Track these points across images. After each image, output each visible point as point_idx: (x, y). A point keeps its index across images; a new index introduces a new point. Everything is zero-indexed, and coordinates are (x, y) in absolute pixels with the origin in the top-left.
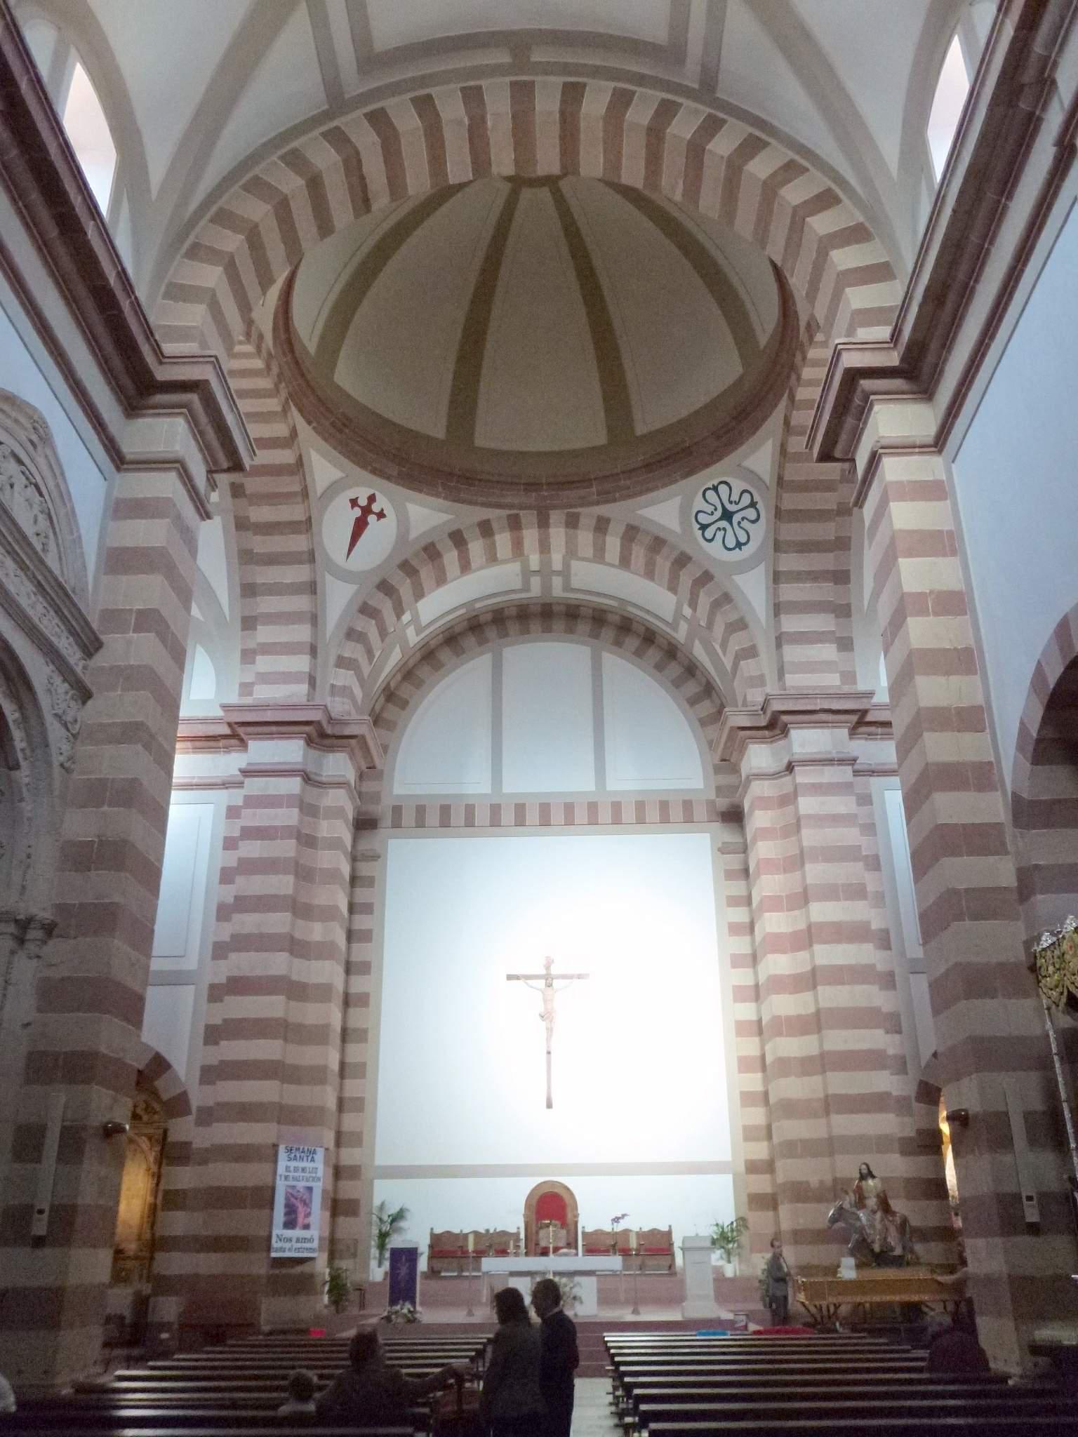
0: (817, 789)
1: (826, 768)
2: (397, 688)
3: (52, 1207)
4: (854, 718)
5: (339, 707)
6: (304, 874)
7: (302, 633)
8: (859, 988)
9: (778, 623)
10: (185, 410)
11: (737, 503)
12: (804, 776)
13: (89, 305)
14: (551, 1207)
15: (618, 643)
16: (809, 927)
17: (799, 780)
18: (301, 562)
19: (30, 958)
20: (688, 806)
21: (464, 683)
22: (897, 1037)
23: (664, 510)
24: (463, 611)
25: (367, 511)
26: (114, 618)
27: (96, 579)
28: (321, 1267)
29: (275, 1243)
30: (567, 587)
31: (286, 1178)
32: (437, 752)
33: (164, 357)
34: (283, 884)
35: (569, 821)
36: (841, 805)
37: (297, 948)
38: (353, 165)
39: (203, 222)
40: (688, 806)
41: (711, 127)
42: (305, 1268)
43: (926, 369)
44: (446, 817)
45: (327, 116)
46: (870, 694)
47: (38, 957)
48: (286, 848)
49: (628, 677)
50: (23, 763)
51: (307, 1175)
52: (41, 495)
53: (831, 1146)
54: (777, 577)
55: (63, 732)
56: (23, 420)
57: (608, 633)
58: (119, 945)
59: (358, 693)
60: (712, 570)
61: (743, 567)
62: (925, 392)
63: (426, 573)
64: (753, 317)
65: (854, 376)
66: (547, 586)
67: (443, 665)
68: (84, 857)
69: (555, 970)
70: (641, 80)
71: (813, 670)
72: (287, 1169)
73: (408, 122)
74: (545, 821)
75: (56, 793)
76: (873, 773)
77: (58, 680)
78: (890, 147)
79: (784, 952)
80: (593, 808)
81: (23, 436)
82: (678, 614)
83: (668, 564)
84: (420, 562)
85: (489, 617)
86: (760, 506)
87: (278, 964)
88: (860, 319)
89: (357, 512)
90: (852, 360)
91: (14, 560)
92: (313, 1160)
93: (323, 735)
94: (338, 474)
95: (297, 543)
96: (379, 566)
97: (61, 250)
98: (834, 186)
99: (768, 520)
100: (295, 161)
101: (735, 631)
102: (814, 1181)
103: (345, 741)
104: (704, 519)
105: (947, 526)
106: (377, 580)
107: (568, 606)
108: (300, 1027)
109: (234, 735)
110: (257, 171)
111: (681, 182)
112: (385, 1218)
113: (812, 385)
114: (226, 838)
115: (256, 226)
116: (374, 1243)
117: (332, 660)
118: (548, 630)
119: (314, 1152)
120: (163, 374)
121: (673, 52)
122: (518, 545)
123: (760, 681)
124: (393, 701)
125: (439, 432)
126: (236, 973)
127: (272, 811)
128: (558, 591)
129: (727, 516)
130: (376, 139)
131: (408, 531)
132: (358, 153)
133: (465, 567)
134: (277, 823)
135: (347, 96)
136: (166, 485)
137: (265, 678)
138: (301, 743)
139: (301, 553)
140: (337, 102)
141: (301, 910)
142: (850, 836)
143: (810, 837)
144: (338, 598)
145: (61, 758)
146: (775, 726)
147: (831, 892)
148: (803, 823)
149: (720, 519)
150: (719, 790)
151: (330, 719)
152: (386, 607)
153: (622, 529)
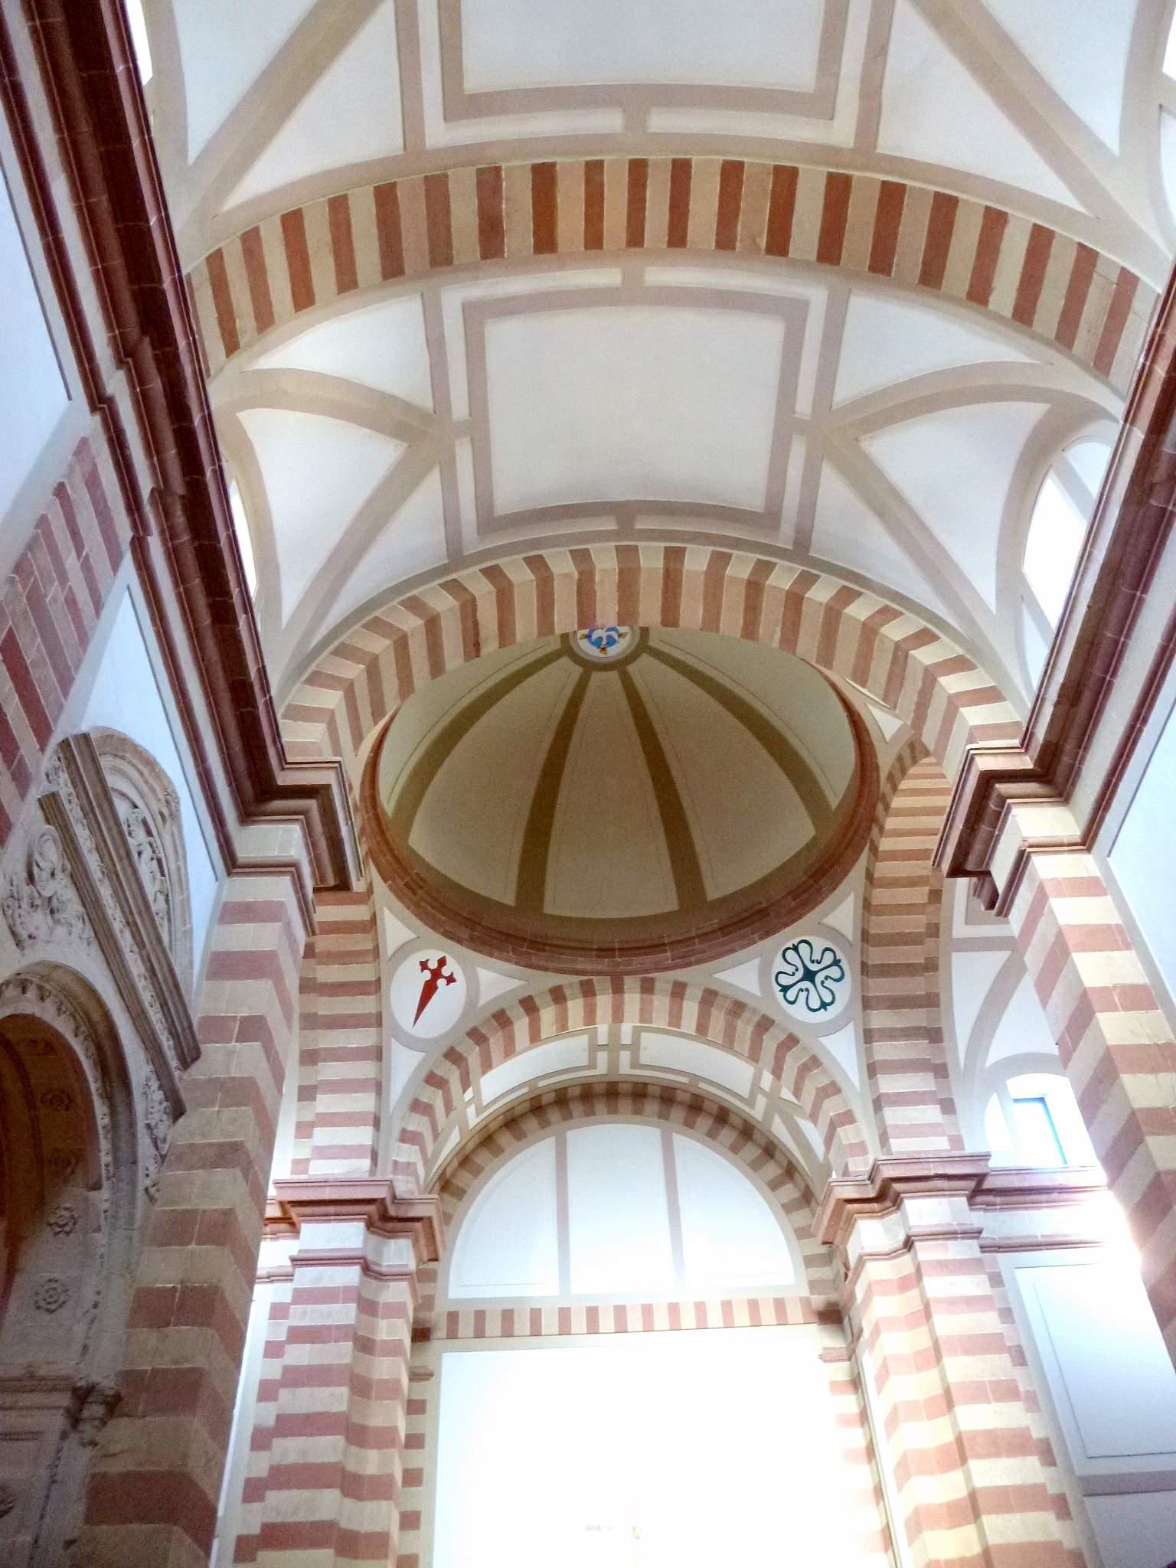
1: (951, 1242)
2: (453, 1175)
4: (971, 1184)
5: (405, 1187)
6: (361, 1387)
7: (365, 1102)
8: (1033, 1517)
9: (874, 1086)
12: (926, 1252)
13: (225, 697)
15: (689, 1124)
16: (959, 1440)
19: (84, 1445)
21: (525, 1170)
23: (742, 973)
24: (525, 1090)
25: (436, 974)
26: (218, 1026)
27: (199, 984)
30: (635, 1064)
32: (499, 1249)
34: (335, 1399)
36: (974, 1285)
37: (353, 1485)
38: (469, 609)
39: (325, 653)
40: (780, 1305)
41: (807, 580)
43: (1061, 769)
46: (986, 1157)
47: (94, 1444)
49: (704, 1163)
50: (106, 1184)
52: (163, 874)
54: (869, 1036)
55: (153, 1151)
56: (158, 789)
57: (678, 1113)
58: (196, 1424)
59: (421, 1172)
60: (798, 1033)
61: (833, 1027)
62: (1060, 795)
63: (496, 1042)
64: (822, 782)
65: (989, 779)
66: (614, 1063)
67: (503, 1151)
68: (159, 1309)
70: (738, 544)
71: (917, 1135)
73: (521, 576)
75: (137, 1225)
76: (999, 1248)
78: (985, 583)
82: (756, 1088)
83: (750, 1029)
84: (488, 1032)
85: (552, 1096)
88: (992, 726)
89: (427, 975)
90: (985, 764)
91: (133, 936)
93: (385, 1217)
95: (364, 1005)
96: (454, 1028)
97: (210, 644)
99: (854, 980)
100: (415, 605)
101: (828, 1096)
104: (785, 980)
105: (1116, 919)
106: (444, 1049)
107: (636, 1084)
109: (286, 1219)
111: (779, 629)
113: (918, 816)
114: (268, 1343)
118: (613, 1110)
120: (284, 779)
121: (771, 517)
122: (590, 1016)
123: (861, 1149)
124: (453, 1184)
125: (509, 899)
126: (273, 1518)
127: (325, 1308)
128: (625, 1068)
129: (809, 976)
131: (477, 993)
132: (474, 600)
133: (535, 1037)
136: (280, 889)
137: (321, 1153)
138: (361, 1225)
140: (456, 558)
142: (989, 1322)
143: (948, 1325)
144: (404, 1067)
145: (148, 1182)
146: (885, 1196)
147: (979, 1393)
149: (802, 980)
150: (813, 1285)
151: (394, 1197)
152: (436, 1098)
153: (700, 994)
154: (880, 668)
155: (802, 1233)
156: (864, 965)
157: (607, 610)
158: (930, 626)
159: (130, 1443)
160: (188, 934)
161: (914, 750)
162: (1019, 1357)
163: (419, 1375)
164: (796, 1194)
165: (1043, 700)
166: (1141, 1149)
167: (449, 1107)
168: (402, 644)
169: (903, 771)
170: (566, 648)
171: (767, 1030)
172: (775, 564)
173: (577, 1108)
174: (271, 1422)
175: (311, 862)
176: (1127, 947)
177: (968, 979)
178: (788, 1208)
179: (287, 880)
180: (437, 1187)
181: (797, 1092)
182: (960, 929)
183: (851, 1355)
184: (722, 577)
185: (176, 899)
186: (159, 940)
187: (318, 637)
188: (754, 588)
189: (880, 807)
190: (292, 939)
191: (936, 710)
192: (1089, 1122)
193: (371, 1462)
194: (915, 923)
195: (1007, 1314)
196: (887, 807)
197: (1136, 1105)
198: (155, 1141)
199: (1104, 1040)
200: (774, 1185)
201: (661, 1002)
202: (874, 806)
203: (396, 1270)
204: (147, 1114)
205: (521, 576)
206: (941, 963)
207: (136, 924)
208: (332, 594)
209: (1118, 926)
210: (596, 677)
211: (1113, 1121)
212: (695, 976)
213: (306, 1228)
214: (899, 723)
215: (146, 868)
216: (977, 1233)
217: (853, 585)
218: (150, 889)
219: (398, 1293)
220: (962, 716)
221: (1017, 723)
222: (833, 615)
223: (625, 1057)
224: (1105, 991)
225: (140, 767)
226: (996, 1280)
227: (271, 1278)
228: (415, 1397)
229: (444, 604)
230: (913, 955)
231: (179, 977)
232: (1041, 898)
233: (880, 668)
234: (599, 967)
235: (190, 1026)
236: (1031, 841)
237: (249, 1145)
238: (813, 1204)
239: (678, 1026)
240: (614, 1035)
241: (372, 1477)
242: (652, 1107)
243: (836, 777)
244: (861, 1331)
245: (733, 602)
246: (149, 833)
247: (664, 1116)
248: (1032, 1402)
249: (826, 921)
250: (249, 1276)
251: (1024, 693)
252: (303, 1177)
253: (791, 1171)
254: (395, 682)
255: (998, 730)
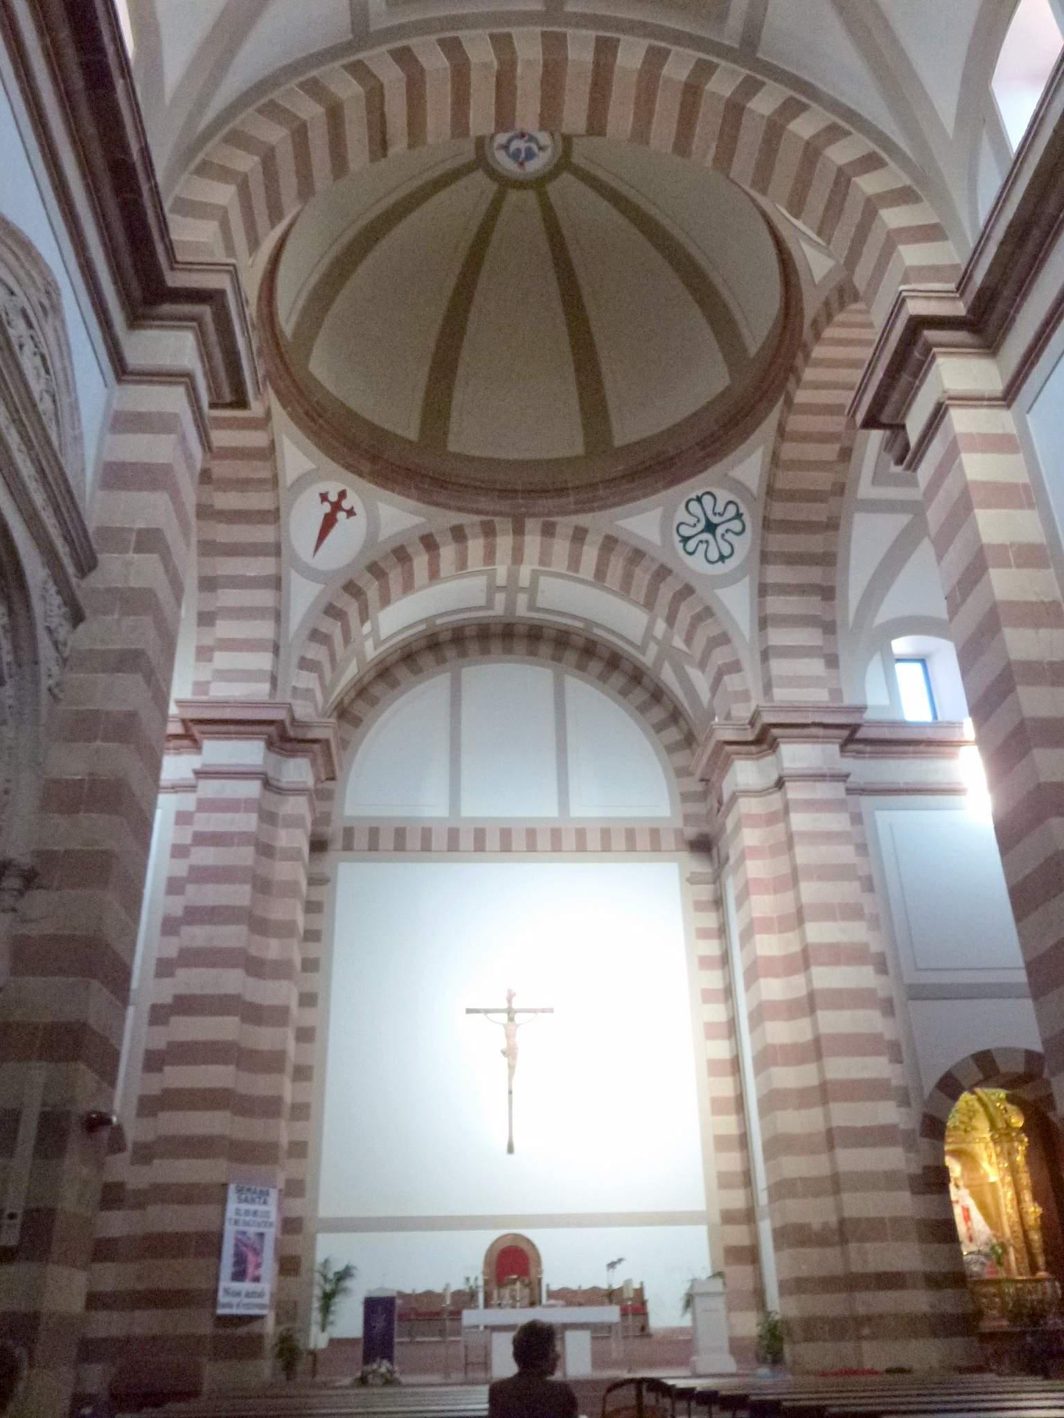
0: (812, 805)
1: (818, 784)
3: (27, 1212)
4: (845, 733)
5: (303, 711)
6: (263, 886)
7: (264, 629)
8: (861, 1014)
10: (195, 324)
11: (721, 515)
12: (795, 792)
14: (513, 1263)
15: (581, 667)
17: (791, 795)
18: (266, 555)
20: (655, 834)
22: (898, 1066)
23: (645, 521)
24: (422, 627)
25: (336, 507)
26: (115, 537)
28: (270, 1327)
29: (222, 1298)
30: (532, 606)
31: (236, 1222)
32: (394, 770)
33: (177, 262)
34: (239, 895)
35: (532, 847)
36: (836, 822)
37: (256, 967)
40: (655, 834)
41: (750, 87)
42: (255, 1327)
43: (994, 318)
44: (402, 841)
45: (348, 48)
47: (14, 910)
48: (244, 856)
49: (591, 701)
51: (259, 1219)
52: (47, 372)
53: (836, 1184)
54: (763, 590)
55: (54, 654)
57: (571, 656)
60: (694, 583)
61: (729, 580)
62: (989, 347)
65: (918, 324)
66: (511, 604)
68: (68, 797)
69: (516, 1005)
70: (679, 38)
71: (800, 685)
72: (238, 1212)
73: (435, 62)
74: (506, 847)
75: (43, 721)
77: (53, 589)
79: (777, 976)
80: (556, 835)
81: (34, 300)
82: (649, 634)
83: (648, 577)
84: (388, 566)
86: (746, 518)
87: (232, 981)
88: (925, 270)
89: (327, 508)
90: (916, 307)
91: (20, 433)
92: (265, 1203)
94: (310, 466)
95: (264, 534)
96: (348, 565)
97: (84, 110)
98: (878, 150)
100: (315, 89)
102: (816, 1222)
103: (308, 746)
104: (686, 531)
105: (1023, 478)
106: (343, 581)
108: (253, 1053)
109: (188, 736)
110: (275, 95)
111: (714, 145)
112: (331, 1276)
113: (837, 366)
115: (272, 149)
116: (316, 1304)
117: (295, 661)
118: (508, 651)
119: (268, 1194)
120: (175, 280)
122: (490, 556)
123: (745, 696)
124: (352, 710)
125: (412, 434)
126: (182, 990)
128: (522, 611)
129: (711, 527)
130: (401, 74)
132: (382, 86)
134: (233, 829)
135: (372, 29)
136: (173, 400)
137: (225, 675)
139: (266, 545)
141: (260, 926)
142: (845, 854)
144: (303, 597)
145: (51, 682)
146: (764, 740)
147: (827, 912)
148: (796, 839)
149: (702, 532)
150: (687, 818)
151: (293, 720)
152: (353, 609)
153: (600, 539)
154: (817, 199)
155: (682, 772)
156: (765, 519)
157: (528, 111)
158: (878, 150)
159: (46, 911)
160: (78, 439)
161: (845, 294)
162: (868, 885)
163: (317, 881)
164: (679, 737)
165: (988, 238)
166: (1010, 698)
167: (347, 638)
168: (300, 134)
169: (830, 317)
170: (482, 161)
171: (664, 578)
172: (717, 66)
173: (473, 647)
174: (179, 912)
175: (205, 375)
176: (1031, 506)
177: (868, 539)
178: (671, 749)
179: (180, 391)
180: (335, 714)
181: (688, 640)
182: (866, 489)
183: (717, 879)
184: (658, 77)
185: (64, 401)
186: (48, 442)
187: (210, 115)
188: (692, 92)
189: (800, 355)
190: (188, 457)
191: (875, 241)
192: (965, 672)
193: (272, 949)
194: (821, 480)
195: (862, 848)
196: (807, 356)
197: (1013, 657)
198: (56, 644)
199: (993, 594)
200: (659, 728)
201: (561, 547)
202: (794, 356)
203: (294, 786)
204: (46, 616)
205: (435, 62)
206: (843, 523)
207: (21, 421)
208: (222, 66)
209: (1025, 486)
210: (513, 196)
211: (989, 668)
212: (597, 522)
213: (208, 745)
214: (830, 263)
215: (29, 363)
216: (844, 777)
217: (802, 94)
218: (37, 387)
219: (297, 806)
220: (900, 256)
221: (956, 267)
222: (774, 131)
223: (522, 599)
224: (1002, 548)
225: (15, 248)
226: (857, 819)
227: (175, 788)
228: (313, 898)
229: (348, 90)
230: (818, 512)
231: (72, 482)
232: (953, 452)
233: (817, 199)
234: (498, 508)
235: (88, 540)
236: (952, 394)
237: (150, 653)
238: (694, 745)
239: (577, 571)
240: (513, 576)
241: (275, 962)
242: (545, 649)
243: (757, 321)
244: (727, 858)
245: (667, 108)
246: (30, 325)
247: (557, 658)
248: (875, 923)
249: (731, 474)
250: (155, 786)
251: (966, 224)
252: (204, 698)
253: (676, 716)
254: (294, 180)
255: (934, 272)
